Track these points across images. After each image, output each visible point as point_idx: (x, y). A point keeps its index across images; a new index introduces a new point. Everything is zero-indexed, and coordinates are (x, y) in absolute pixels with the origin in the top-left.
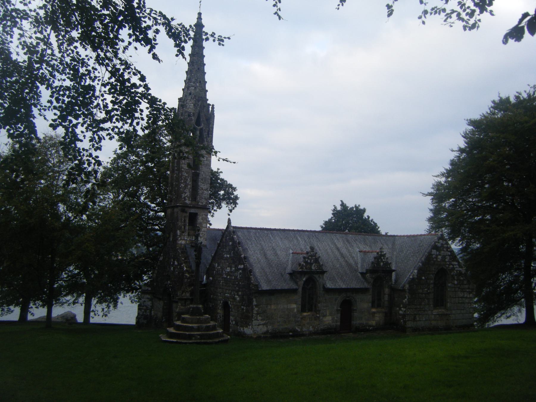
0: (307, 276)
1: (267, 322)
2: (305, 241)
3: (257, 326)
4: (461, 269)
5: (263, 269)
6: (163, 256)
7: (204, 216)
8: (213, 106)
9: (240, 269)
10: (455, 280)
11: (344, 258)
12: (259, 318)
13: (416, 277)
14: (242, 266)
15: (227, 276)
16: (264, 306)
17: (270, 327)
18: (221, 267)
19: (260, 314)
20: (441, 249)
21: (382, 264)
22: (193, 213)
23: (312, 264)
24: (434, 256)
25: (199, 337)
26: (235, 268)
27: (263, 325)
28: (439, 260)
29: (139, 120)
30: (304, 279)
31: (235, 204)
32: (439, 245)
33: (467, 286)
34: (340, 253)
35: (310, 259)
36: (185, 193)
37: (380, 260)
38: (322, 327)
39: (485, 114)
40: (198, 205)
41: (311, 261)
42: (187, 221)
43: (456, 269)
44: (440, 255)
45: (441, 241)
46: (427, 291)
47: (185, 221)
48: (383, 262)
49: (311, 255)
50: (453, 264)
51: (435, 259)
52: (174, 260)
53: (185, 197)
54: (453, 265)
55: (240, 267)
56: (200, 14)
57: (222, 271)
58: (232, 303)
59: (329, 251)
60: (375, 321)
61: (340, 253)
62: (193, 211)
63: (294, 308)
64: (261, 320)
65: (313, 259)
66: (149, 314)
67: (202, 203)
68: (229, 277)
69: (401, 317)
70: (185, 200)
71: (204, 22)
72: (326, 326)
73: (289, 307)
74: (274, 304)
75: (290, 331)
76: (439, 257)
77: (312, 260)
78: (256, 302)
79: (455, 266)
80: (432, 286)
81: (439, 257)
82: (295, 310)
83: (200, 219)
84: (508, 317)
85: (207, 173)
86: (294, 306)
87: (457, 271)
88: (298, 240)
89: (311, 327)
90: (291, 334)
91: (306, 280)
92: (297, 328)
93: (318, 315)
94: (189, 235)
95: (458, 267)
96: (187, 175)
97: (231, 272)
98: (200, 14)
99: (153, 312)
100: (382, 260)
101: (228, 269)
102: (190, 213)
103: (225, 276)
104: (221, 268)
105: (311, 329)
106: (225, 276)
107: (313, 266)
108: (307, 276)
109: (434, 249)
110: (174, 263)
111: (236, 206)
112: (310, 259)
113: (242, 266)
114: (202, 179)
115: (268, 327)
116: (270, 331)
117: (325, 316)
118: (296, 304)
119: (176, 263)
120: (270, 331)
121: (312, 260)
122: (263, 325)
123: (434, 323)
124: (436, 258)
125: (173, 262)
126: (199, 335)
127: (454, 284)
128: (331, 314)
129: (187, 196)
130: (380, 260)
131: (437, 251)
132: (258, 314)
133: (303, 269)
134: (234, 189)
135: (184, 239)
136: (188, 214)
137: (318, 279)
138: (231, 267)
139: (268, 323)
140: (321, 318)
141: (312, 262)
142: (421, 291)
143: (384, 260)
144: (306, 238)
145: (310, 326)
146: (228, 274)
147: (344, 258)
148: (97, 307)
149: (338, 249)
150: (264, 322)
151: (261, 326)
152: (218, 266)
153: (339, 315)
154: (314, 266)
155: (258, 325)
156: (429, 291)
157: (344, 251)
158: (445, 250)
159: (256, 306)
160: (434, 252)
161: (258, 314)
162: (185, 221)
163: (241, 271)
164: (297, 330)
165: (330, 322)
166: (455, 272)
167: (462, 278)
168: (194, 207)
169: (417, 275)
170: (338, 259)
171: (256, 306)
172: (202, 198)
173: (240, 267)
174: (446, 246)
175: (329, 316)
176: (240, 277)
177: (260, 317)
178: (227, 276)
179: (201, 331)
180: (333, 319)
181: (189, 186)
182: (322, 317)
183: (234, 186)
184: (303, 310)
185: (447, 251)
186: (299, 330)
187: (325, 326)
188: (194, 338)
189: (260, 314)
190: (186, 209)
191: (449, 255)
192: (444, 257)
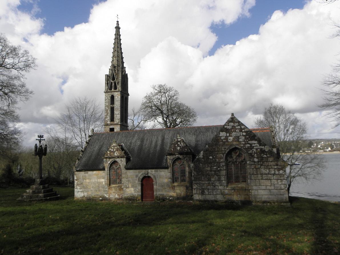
1: (83, 190)
3: (77, 193)
10: (255, 157)
12: (78, 187)
16: (81, 180)
17: (86, 193)
19: (79, 185)
20: (232, 130)
21: (179, 148)
22: (112, 128)
23: (115, 152)
27: (81, 192)
35: (112, 149)
36: (107, 118)
37: (176, 145)
38: (125, 196)
41: (113, 150)
46: (217, 169)
48: (180, 147)
49: (114, 146)
50: (250, 143)
53: (107, 120)
56: (118, 22)
60: (175, 193)
62: (111, 127)
63: (103, 182)
64: (80, 189)
65: (115, 148)
67: (116, 122)
70: (107, 121)
71: (120, 26)
72: (129, 195)
73: (99, 181)
74: (88, 179)
75: (101, 197)
77: (115, 149)
78: (76, 177)
82: (104, 183)
84: (106, 195)
85: (118, 105)
86: (103, 180)
89: (116, 195)
92: (105, 195)
95: (258, 145)
96: (108, 108)
98: (118, 22)
107: (115, 153)
109: (222, 132)
112: (112, 149)
114: (116, 109)
115: (85, 193)
116: (86, 196)
118: (104, 179)
120: (86, 196)
121: (115, 149)
122: (81, 192)
127: (255, 162)
129: (108, 120)
130: (176, 145)
131: (227, 133)
132: (77, 185)
133: (108, 155)
139: (84, 191)
141: (114, 151)
143: (180, 145)
145: (116, 194)
150: (82, 190)
151: (80, 193)
154: (117, 153)
155: (78, 192)
156: (219, 169)
159: (76, 180)
161: (77, 185)
164: (105, 196)
165: (133, 192)
166: (255, 150)
171: (76, 180)
172: (116, 119)
175: (131, 188)
177: (79, 187)
181: (109, 114)
182: (125, 188)
186: (107, 197)
187: (128, 195)
189: (79, 185)
191: (243, 136)
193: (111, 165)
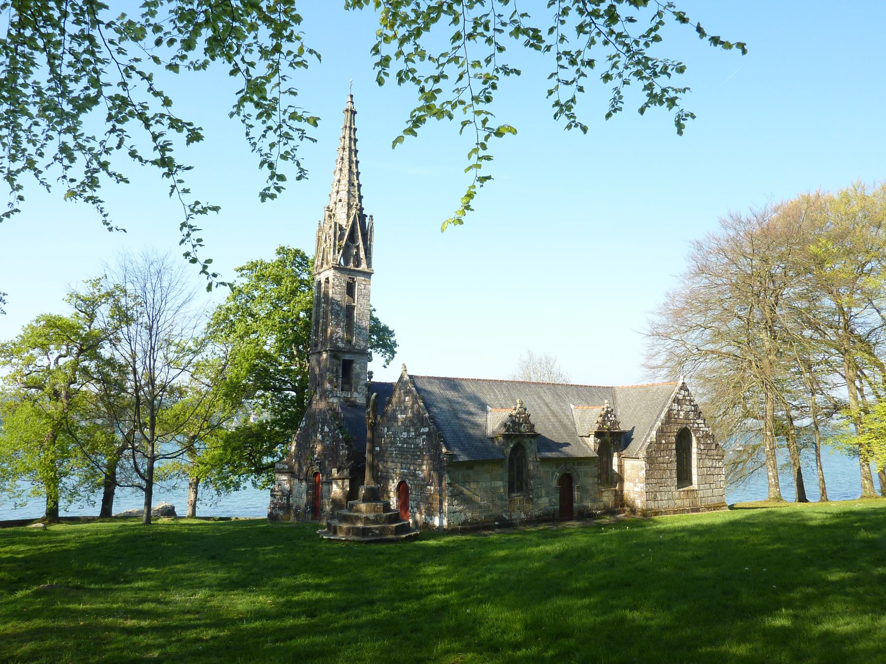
0: (515, 442)
2: (504, 394)
4: (707, 429)
5: (455, 433)
6: (306, 421)
7: (362, 364)
8: (371, 216)
9: (423, 434)
11: (556, 416)
13: (655, 440)
14: (427, 430)
15: (403, 444)
18: (393, 432)
24: (675, 412)
25: (377, 532)
26: (415, 432)
28: (681, 417)
29: (493, 81)
30: (512, 446)
31: (393, 353)
32: (681, 397)
33: (715, 452)
34: (551, 410)
39: (811, 195)
40: (354, 349)
41: (519, 420)
42: (340, 371)
43: (702, 429)
44: (682, 410)
45: (682, 392)
47: (337, 371)
48: (611, 421)
51: (676, 417)
52: (323, 426)
53: (337, 338)
54: (698, 424)
55: (422, 430)
57: (395, 438)
58: (411, 482)
59: (537, 408)
61: (551, 410)
62: (347, 357)
66: (285, 502)
68: (405, 446)
69: (637, 495)
74: (474, 481)
76: (682, 413)
79: (700, 426)
80: (674, 452)
81: (682, 413)
83: (357, 367)
86: (500, 483)
87: (703, 431)
88: (495, 393)
90: (497, 523)
91: (515, 447)
92: (504, 515)
93: (531, 496)
94: (342, 390)
97: (410, 438)
99: (291, 499)
100: (608, 418)
101: (405, 435)
102: (344, 361)
103: (400, 445)
104: (394, 433)
105: (523, 516)
106: (400, 445)
108: (515, 442)
110: (323, 429)
111: (394, 356)
113: (427, 430)
117: (539, 497)
119: (326, 429)
123: (679, 502)
124: (678, 414)
125: (321, 428)
126: (377, 529)
128: (547, 494)
134: (391, 333)
135: (337, 396)
136: (341, 362)
137: (529, 445)
138: (409, 432)
140: (535, 499)
142: (661, 459)
144: (505, 391)
146: (404, 441)
147: (556, 416)
148: (207, 494)
149: (547, 405)
152: (388, 431)
153: (558, 495)
154: (524, 428)
157: (554, 407)
158: (687, 403)
160: (675, 406)
162: (337, 371)
163: (424, 437)
167: (709, 442)
168: (349, 352)
169: (656, 438)
170: (549, 419)
173: (422, 430)
174: (688, 398)
176: (423, 445)
178: (403, 444)
179: (380, 524)
180: (550, 501)
183: (391, 329)
184: (511, 490)
185: (690, 404)
188: (370, 534)
190: (339, 354)
192: (687, 413)
193: (514, 450)
